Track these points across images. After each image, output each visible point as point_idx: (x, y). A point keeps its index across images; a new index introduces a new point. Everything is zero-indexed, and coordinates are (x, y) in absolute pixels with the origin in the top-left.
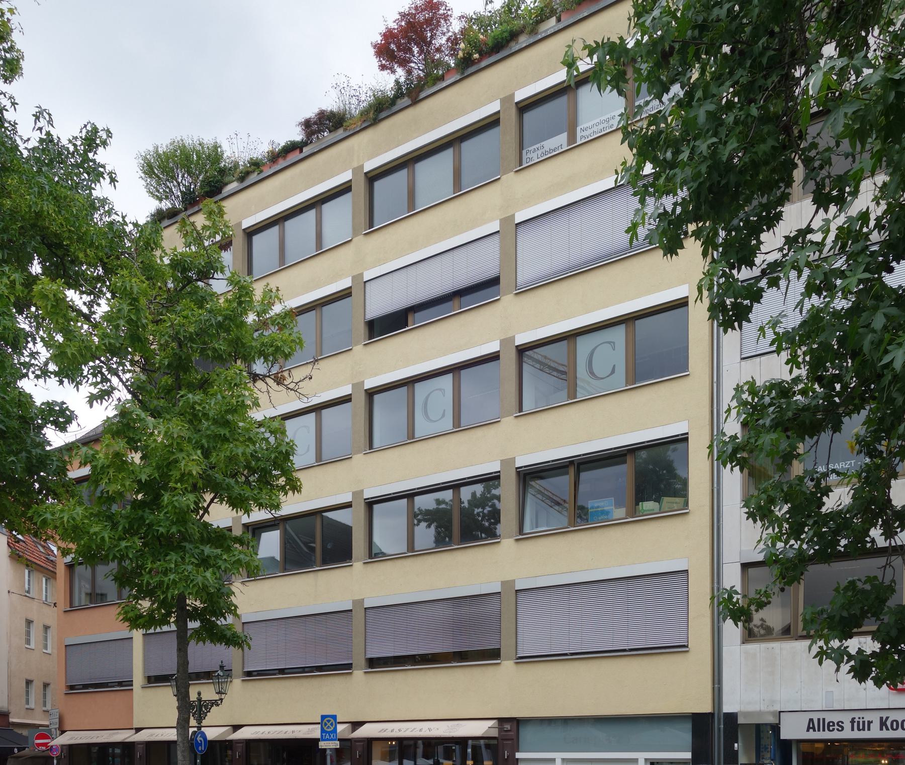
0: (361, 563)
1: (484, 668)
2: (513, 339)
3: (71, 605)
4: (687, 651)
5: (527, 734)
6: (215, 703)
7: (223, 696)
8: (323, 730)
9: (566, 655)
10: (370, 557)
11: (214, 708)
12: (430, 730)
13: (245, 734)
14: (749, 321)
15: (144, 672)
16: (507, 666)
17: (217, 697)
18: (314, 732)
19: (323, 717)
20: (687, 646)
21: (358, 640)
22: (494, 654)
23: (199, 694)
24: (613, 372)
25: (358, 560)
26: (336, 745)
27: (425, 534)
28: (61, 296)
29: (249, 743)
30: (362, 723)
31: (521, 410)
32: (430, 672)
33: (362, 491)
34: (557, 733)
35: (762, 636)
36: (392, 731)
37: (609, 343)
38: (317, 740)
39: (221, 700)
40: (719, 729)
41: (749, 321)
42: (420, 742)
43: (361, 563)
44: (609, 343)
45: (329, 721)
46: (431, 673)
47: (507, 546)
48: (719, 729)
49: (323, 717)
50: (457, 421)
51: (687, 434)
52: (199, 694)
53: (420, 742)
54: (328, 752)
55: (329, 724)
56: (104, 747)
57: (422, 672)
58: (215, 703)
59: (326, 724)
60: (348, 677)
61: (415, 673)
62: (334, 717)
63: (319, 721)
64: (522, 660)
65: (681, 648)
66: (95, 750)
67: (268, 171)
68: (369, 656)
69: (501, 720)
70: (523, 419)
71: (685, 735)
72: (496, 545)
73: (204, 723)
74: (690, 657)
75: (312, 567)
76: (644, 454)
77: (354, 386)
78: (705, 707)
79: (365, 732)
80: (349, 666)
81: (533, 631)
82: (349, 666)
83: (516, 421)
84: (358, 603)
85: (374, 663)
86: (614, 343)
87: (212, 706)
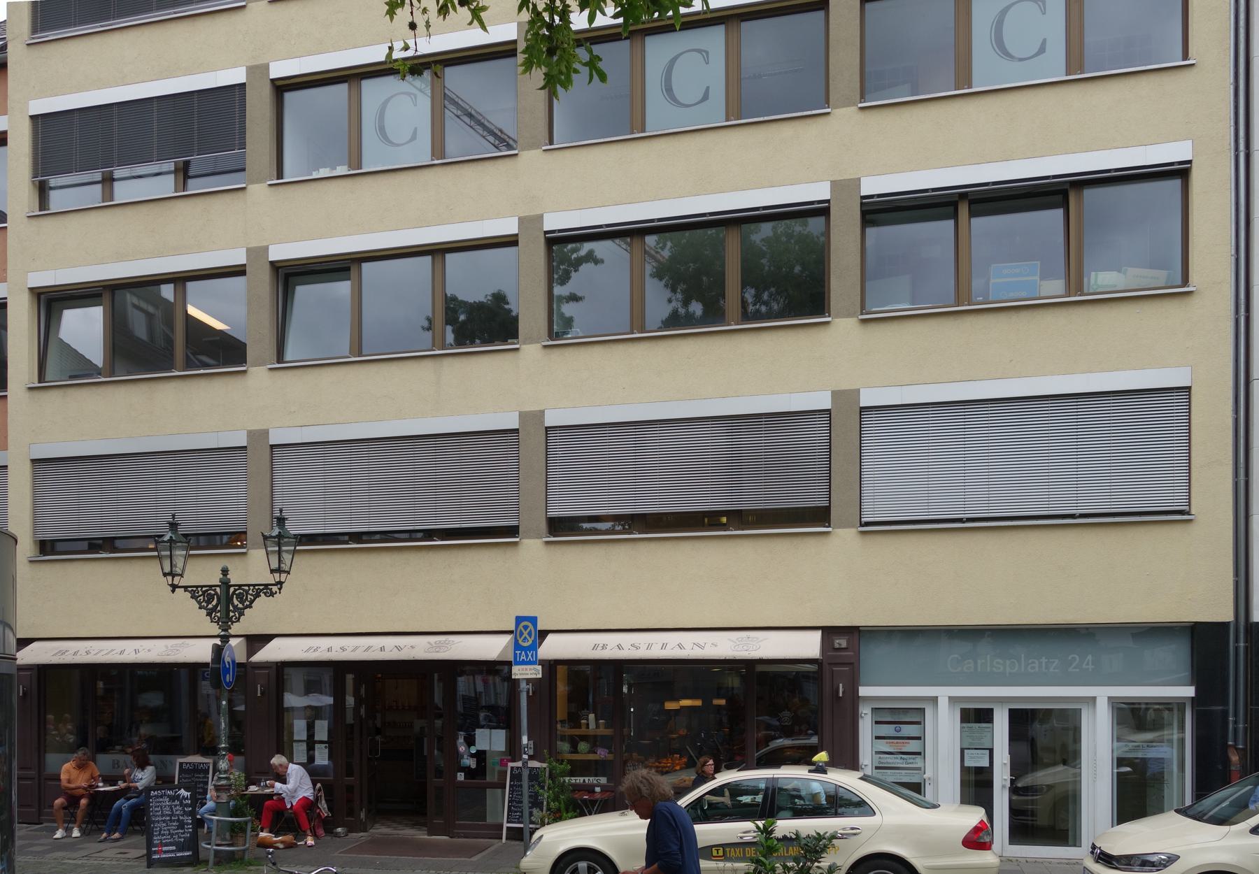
0: (538, 346)
1: (796, 541)
2: (266, 68)
3: (41, 378)
5: (873, 656)
7: (284, 576)
8: (517, 646)
9: (1072, 516)
10: (551, 337)
15: (35, 533)
16: (843, 538)
17: (270, 579)
18: (491, 648)
19: (519, 620)
20: (1188, 513)
21: (531, 484)
22: (820, 516)
23: (225, 572)
24: (1042, 50)
25: (531, 340)
26: (535, 672)
27: (659, 301)
29: (44, 672)
30: (267, 638)
31: (280, 175)
33: (266, 249)
34: (951, 653)
36: (75, 654)
37: (699, 51)
38: (509, 664)
39: (280, 583)
40: (1237, 649)
42: (561, 671)
43: (538, 346)
44: (699, 51)
45: (526, 627)
46: (686, 547)
47: (258, 377)
48: (1237, 649)
49: (519, 620)
50: (1075, 58)
51: (1190, 162)
52: (225, 572)
53: (183, 672)
54: (523, 685)
55: (526, 634)
57: (668, 545)
58: (266, 590)
59: (521, 634)
60: (509, 552)
62: (533, 620)
63: (513, 628)
64: (869, 528)
65: (1180, 515)
68: (550, 514)
69: (829, 632)
70: (281, 188)
71: (1176, 655)
72: (822, 328)
74: (1194, 531)
75: (169, 369)
76: (766, 229)
77: (251, 70)
78: (1223, 612)
79: (273, 652)
80: (512, 531)
81: (890, 480)
82: (512, 531)
83: (862, 115)
84: (259, 436)
85: (560, 527)
86: (707, 53)
87: (258, 595)
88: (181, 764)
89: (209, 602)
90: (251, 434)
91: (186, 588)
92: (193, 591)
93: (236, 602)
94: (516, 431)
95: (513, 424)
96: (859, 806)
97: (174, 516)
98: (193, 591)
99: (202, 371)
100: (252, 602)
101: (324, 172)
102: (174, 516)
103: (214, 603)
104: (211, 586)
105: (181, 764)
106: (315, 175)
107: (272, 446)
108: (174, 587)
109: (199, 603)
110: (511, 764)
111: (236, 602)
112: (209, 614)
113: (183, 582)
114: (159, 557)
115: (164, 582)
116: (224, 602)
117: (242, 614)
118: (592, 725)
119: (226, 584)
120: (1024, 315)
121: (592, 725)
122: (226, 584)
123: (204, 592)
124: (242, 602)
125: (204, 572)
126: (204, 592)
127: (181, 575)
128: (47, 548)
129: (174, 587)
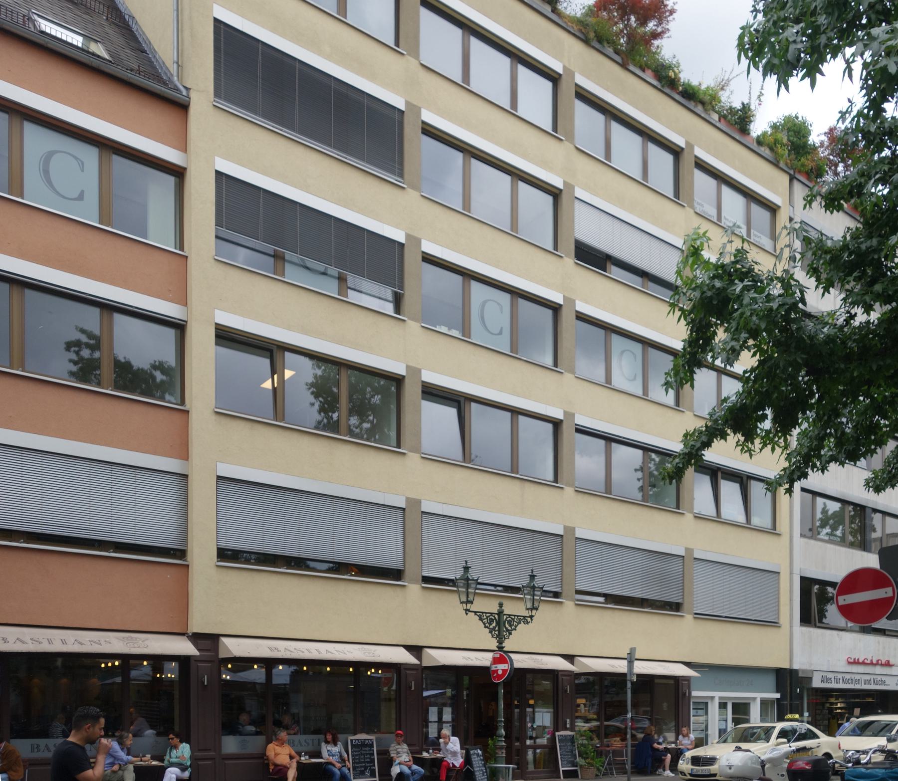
4: (682, 616)
6: (525, 620)
7: (534, 612)
11: (522, 626)
12: (613, 666)
13: (641, 668)
14: (822, 74)
17: (527, 613)
18: (620, 667)
22: (676, 607)
23: (501, 605)
28: (775, 70)
32: (634, 615)
35: (351, 433)
39: (531, 617)
41: (822, 74)
56: (361, 666)
57: (627, 613)
61: (621, 613)
66: (59, 662)
67: (840, 676)
71: (771, 680)
73: (508, 645)
88: (352, 741)
89: (490, 624)
90: (408, 500)
91: (475, 612)
92: (480, 615)
93: (507, 626)
94: (561, 536)
95: (561, 532)
96: (815, 736)
97: (466, 562)
98: (480, 615)
99: (373, 444)
100: (516, 626)
101: (444, 329)
102: (466, 562)
103: (494, 624)
104: (492, 614)
105: (352, 741)
106: (437, 329)
107: (423, 512)
108: (467, 611)
109: (484, 624)
110: (557, 734)
111: (507, 626)
112: (491, 632)
113: (473, 608)
114: (457, 592)
115: (460, 608)
116: (500, 625)
117: (510, 634)
118: (583, 711)
119: (500, 613)
120: (586, 496)
121: (583, 711)
122: (500, 613)
123: (487, 617)
124: (511, 626)
125: (491, 606)
126: (487, 617)
127: (472, 603)
128: (226, 555)
129: (467, 611)
